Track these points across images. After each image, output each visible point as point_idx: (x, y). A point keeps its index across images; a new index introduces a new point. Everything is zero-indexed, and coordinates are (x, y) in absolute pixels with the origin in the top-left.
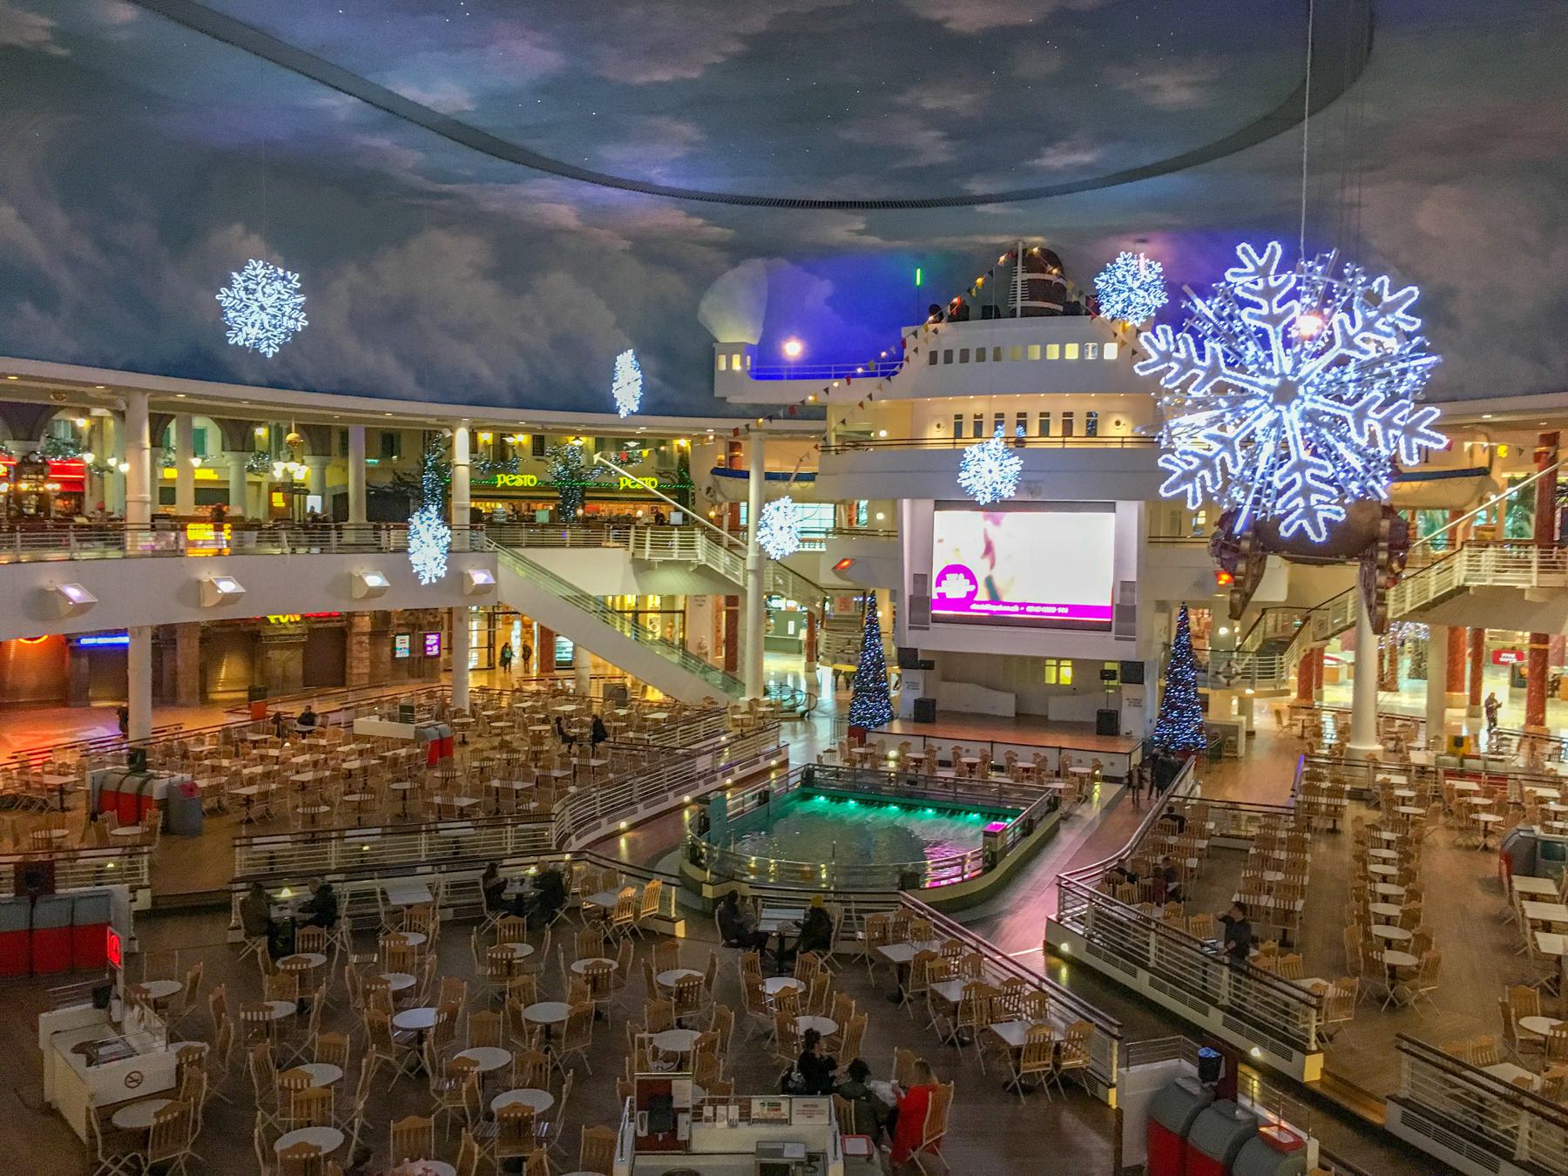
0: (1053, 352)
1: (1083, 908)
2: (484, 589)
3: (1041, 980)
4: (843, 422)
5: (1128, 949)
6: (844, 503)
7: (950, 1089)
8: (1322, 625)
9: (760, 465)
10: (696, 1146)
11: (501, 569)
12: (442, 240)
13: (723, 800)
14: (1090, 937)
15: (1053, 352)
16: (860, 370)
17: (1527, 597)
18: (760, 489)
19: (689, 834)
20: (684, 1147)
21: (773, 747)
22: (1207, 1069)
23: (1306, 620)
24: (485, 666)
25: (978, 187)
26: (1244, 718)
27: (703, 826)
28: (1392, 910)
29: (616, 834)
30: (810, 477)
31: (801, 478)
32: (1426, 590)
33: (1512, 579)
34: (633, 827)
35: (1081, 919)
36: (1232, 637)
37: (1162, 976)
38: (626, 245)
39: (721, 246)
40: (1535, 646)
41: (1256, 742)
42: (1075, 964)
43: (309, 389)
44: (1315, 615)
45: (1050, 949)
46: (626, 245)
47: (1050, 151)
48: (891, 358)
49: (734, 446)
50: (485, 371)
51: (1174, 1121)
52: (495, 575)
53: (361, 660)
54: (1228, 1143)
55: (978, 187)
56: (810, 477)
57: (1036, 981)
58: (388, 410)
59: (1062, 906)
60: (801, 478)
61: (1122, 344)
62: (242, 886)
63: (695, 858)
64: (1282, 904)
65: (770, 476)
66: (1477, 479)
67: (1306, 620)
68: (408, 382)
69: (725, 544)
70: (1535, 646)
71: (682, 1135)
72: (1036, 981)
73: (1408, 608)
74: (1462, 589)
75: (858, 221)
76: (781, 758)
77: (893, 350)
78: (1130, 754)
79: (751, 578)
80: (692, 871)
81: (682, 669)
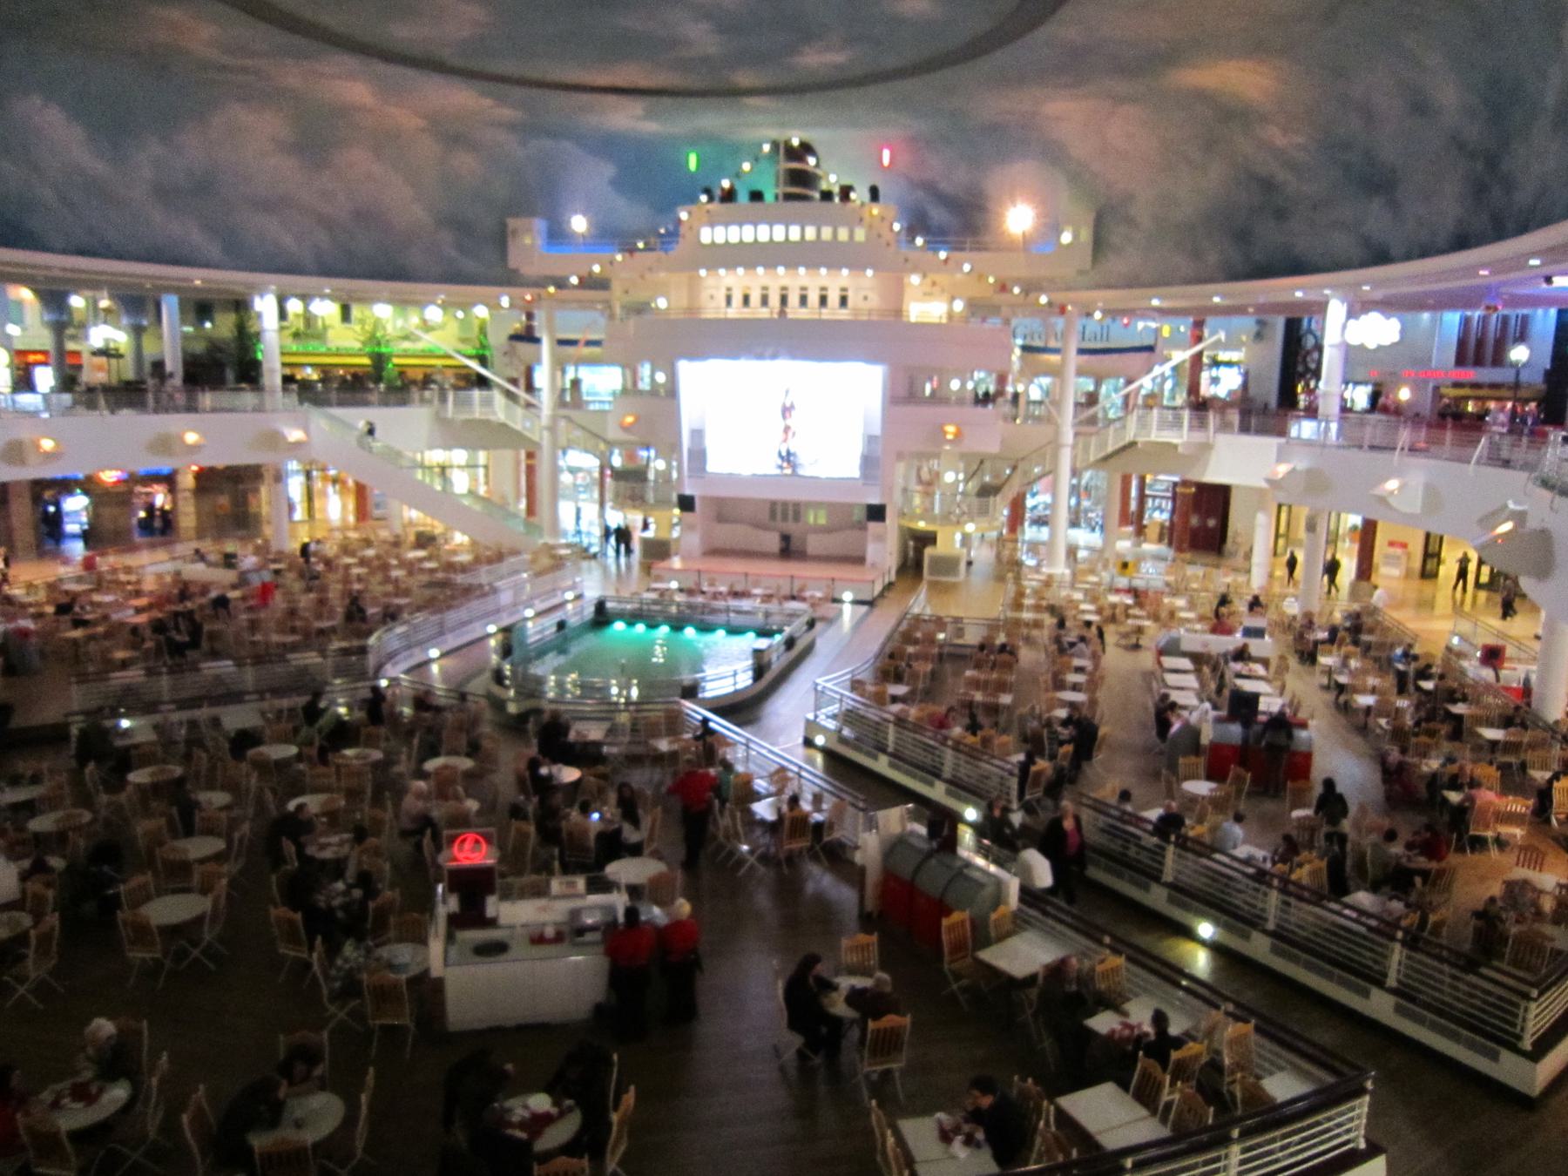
1: (834, 709)
2: (298, 445)
3: (800, 767)
4: (627, 292)
6: (630, 368)
7: (553, 857)
8: (1025, 473)
9: (551, 331)
10: (503, 921)
12: (241, 115)
13: (524, 629)
14: (840, 731)
15: (810, 233)
16: (328, 291)
17: (1180, 450)
21: (569, 583)
22: (934, 830)
23: (1014, 468)
25: (744, 79)
26: (965, 551)
27: (506, 651)
31: (589, 343)
34: (443, 655)
35: (834, 717)
36: (957, 482)
37: (897, 757)
38: (421, 123)
39: (512, 127)
40: (791, 508)
41: (974, 567)
42: (828, 753)
45: (808, 743)
46: (421, 123)
47: (807, 49)
49: (530, 316)
50: (288, 241)
53: (187, 514)
55: (744, 79)
57: (796, 769)
58: (198, 278)
59: (817, 708)
60: (589, 343)
62: (80, 718)
63: (498, 677)
66: (1144, 355)
67: (1014, 468)
68: (214, 251)
69: (522, 402)
70: (791, 508)
71: (490, 911)
72: (796, 769)
73: (1092, 459)
74: (1133, 444)
75: (636, 107)
76: (578, 592)
77: (671, 227)
78: (873, 582)
79: (546, 434)
80: (496, 690)
81: (1354, 454)
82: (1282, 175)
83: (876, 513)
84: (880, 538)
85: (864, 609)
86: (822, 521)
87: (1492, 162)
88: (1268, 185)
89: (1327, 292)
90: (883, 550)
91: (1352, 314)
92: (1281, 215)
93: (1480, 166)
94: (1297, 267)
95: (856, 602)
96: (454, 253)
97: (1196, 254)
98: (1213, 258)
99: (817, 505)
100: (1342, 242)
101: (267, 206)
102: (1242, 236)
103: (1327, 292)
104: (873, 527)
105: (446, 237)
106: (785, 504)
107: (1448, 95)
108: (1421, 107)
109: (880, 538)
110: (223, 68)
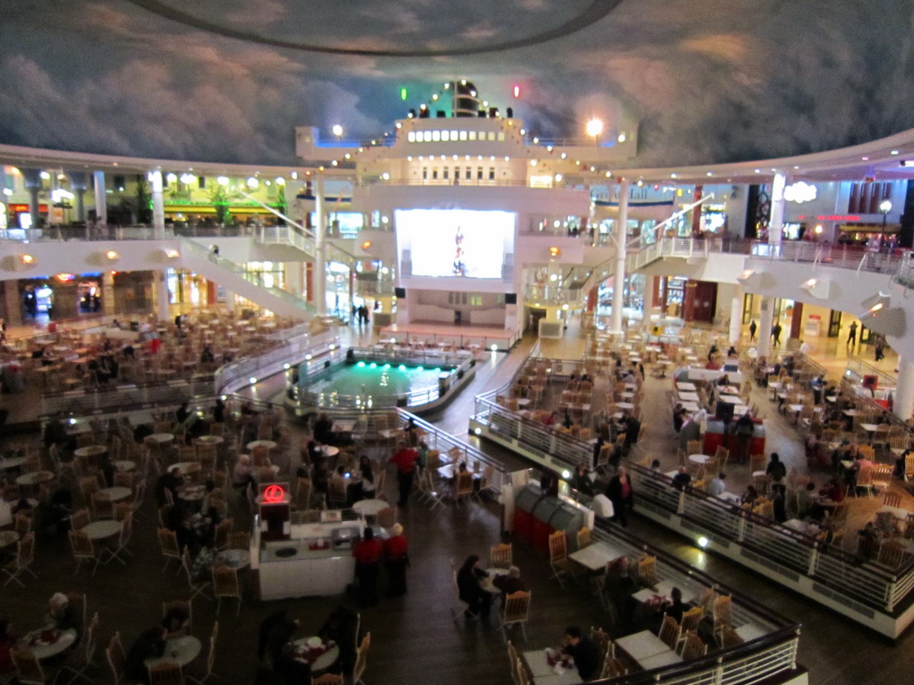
0: (473, 136)
1: (486, 413)
2: (174, 259)
3: (467, 447)
4: (365, 170)
5: (852, 589)
6: (368, 214)
8: (598, 275)
10: (293, 536)
11: (182, 249)
13: (305, 366)
14: (490, 426)
18: (323, 207)
19: (288, 383)
20: (287, 537)
23: (591, 273)
24: (179, 302)
25: (434, 46)
27: (295, 379)
28: (629, 395)
29: (250, 385)
30: (348, 200)
31: (344, 200)
32: (645, 259)
33: (682, 254)
35: (486, 417)
36: (558, 280)
37: (523, 441)
38: (246, 71)
39: (298, 74)
41: (568, 330)
42: (483, 439)
43: (70, 149)
44: (595, 271)
45: (471, 432)
46: (246, 71)
48: (390, 136)
49: (309, 184)
50: (168, 140)
51: (528, 506)
52: (179, 252)
53: (109, 299)
54: (455, 578)
55: (434, 46)
56: (348, 200)
58: (116, 162)
59: (477, 412)
60: (344, 200)
61: (507, 132)
63: (291, 394)
64: (577, 407)
65: (328, 199)
67: (591, 273)
68: (125, 146)
69: (305, 234)
70: (461, 296)
71: (286, 531)
72: (464, 448)
73: (637, 267)
74: (660, 259)
77: (391, 132)
79: (318, 253)
80: (289, 402)
82: (747, 102)
83: (511, 299)
84: (513, 313)
85: (504, 354)
86: (479, 303)
87: (870, 94)
88: (739, 108)
89: (774, 170)
90: (515, 320)
91: (788, 183)
92: (747, 125)
93: (863, 97)
94: (756, 155)
95: (499, 351)
96: (264, 147)
97: (697, 148)
98: (707, 150)
99: (477, 294)
100: (782, 141)
101: (156, 120)
102: (724, 138)
103: (774, 170)
104: (509, 307)
105: (260, 138)
106: (458, 294)
107: (844, 56)
108: (828, 62)
109: (513, 313)
110: (130, 40)
